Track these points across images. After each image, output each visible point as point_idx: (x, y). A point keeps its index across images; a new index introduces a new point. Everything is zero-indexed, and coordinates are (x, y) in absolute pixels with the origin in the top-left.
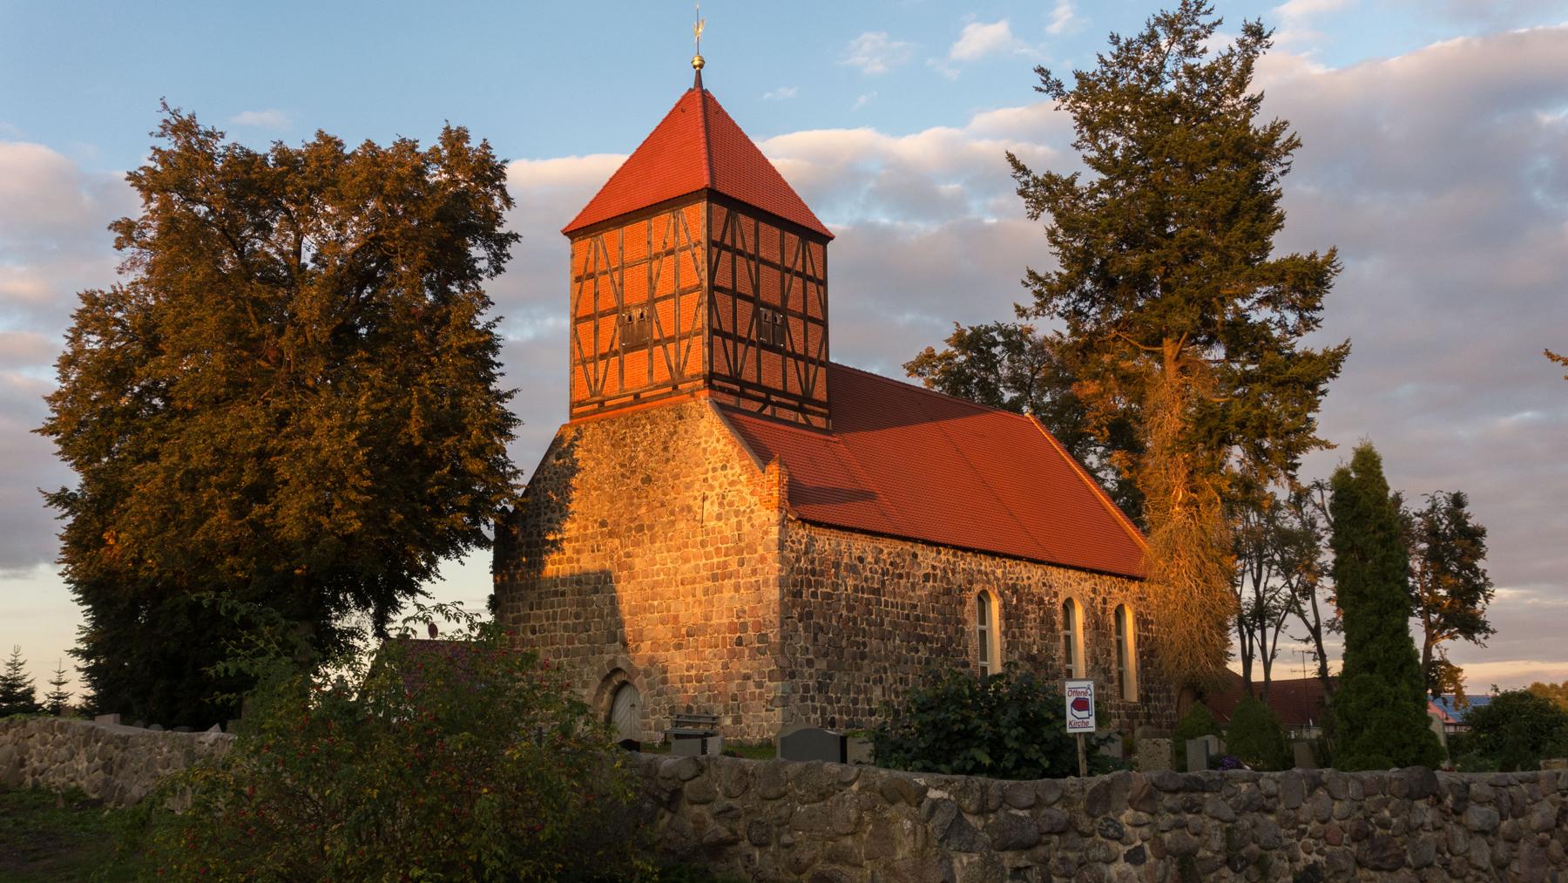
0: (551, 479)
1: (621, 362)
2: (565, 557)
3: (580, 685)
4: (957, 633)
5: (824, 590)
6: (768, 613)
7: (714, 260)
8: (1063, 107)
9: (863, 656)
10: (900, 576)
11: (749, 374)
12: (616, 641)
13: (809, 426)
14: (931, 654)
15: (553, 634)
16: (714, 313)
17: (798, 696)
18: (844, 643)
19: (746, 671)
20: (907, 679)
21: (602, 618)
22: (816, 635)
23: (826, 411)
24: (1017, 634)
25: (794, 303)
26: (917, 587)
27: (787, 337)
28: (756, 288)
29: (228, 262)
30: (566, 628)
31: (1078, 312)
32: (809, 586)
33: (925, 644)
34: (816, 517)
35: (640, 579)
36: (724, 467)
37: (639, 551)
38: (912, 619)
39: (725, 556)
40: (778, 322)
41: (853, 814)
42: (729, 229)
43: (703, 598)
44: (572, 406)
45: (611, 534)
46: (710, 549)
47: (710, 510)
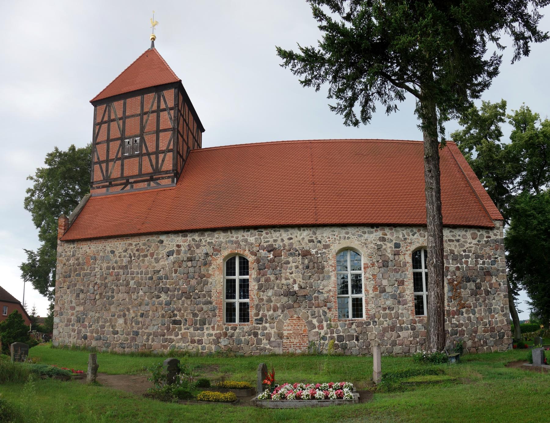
29: (467, 150)
34: (78, 237)
41: (375, 406)
42: (107, 113)
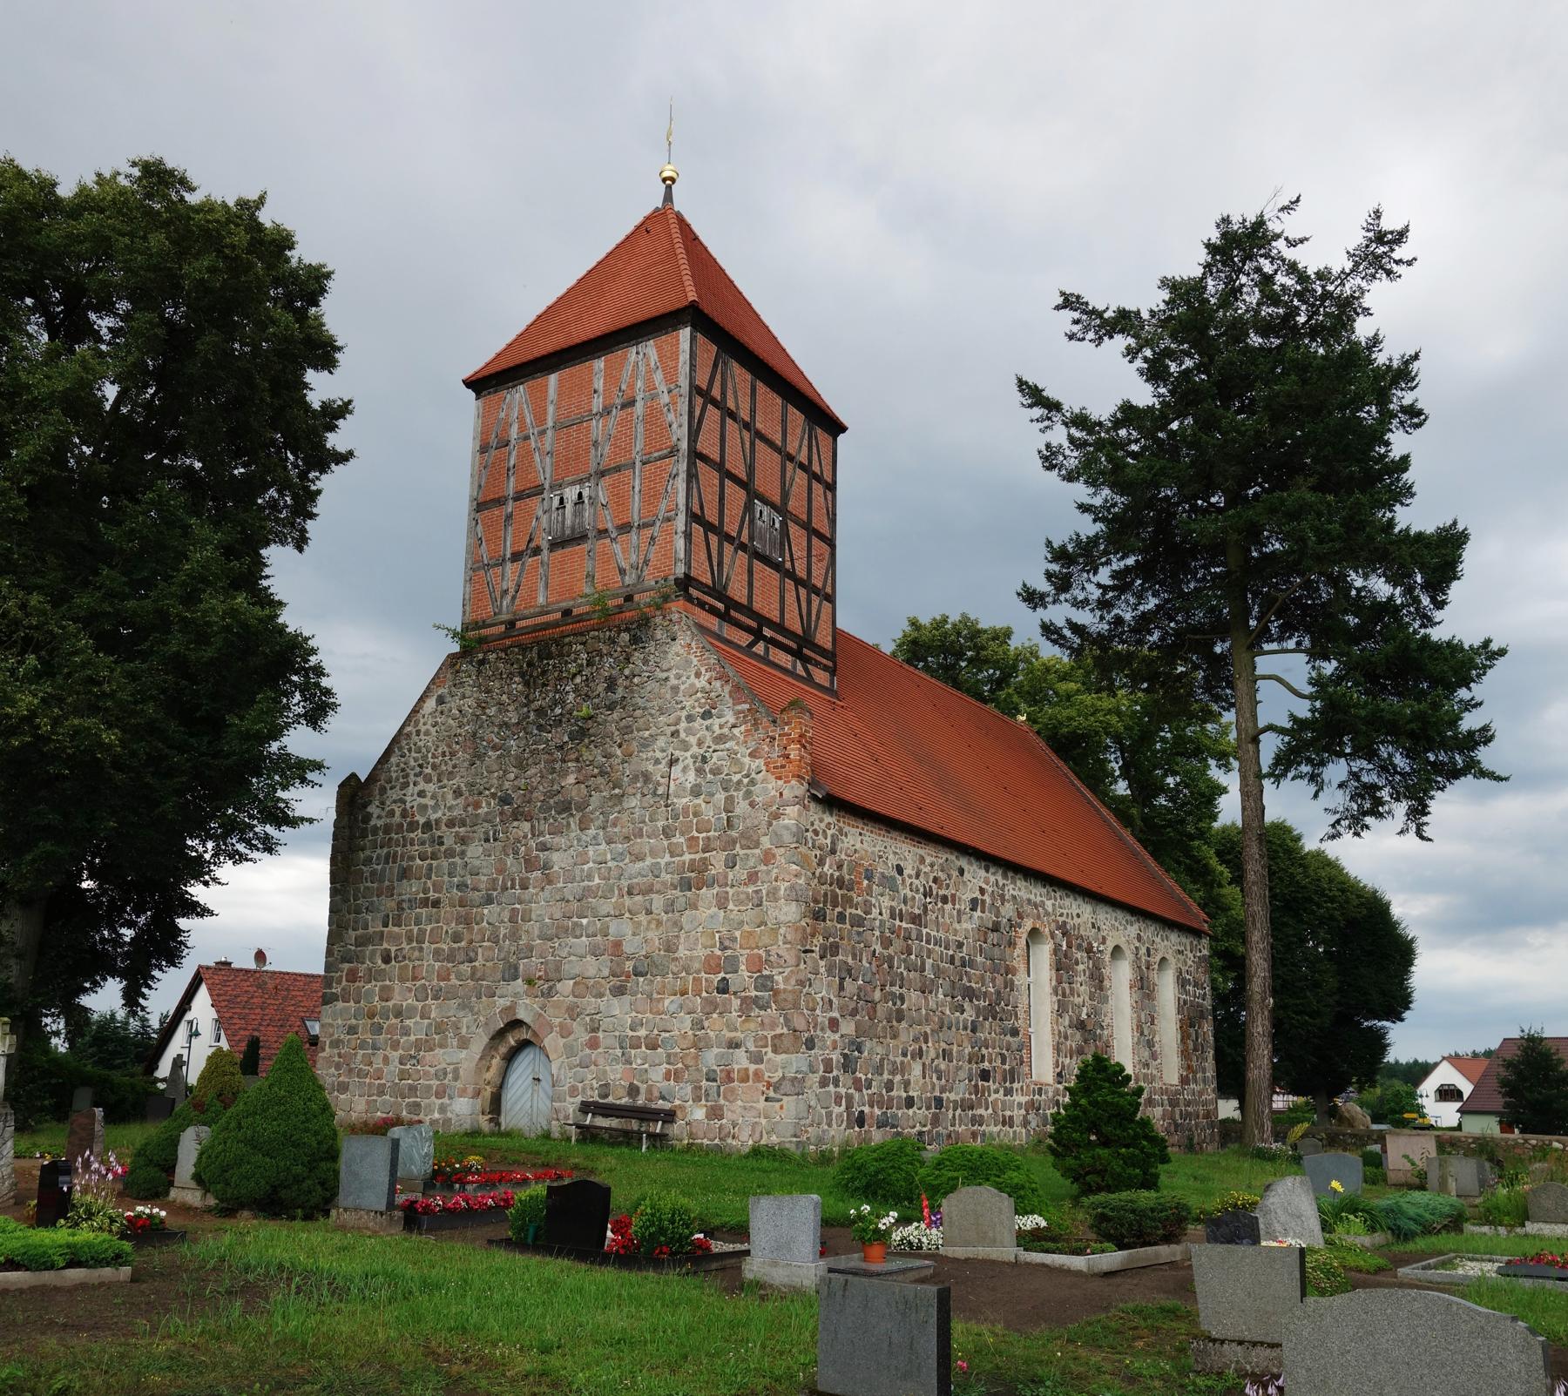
0: (427, 733)
2: (443, 848)
3: (455, 1043)
7: (697, 413)
10: (945, 900)
11: (738, 591)
12: (515, 978)
13: (809, 680)
14: (978, 1017)
16: (695, 490)
17: (816, 1078)
18: (877, 995)
19: (733, 1034)
20: (951, 1053)
21: (497, 943)
22: (842, 979)
24: (1068, 991)
25: (796, 505)
26: (964, 917)
28: (751, 470)
32: (835, 905)
33: (971, 1001)
35: (560, 885)
36: (706, 715)
37: (560, 841)
38: (957, 962)
39: (704, 851)
42: (718, 377)
43: (665, 917)
45: (517, 816)
46: (679, 839)
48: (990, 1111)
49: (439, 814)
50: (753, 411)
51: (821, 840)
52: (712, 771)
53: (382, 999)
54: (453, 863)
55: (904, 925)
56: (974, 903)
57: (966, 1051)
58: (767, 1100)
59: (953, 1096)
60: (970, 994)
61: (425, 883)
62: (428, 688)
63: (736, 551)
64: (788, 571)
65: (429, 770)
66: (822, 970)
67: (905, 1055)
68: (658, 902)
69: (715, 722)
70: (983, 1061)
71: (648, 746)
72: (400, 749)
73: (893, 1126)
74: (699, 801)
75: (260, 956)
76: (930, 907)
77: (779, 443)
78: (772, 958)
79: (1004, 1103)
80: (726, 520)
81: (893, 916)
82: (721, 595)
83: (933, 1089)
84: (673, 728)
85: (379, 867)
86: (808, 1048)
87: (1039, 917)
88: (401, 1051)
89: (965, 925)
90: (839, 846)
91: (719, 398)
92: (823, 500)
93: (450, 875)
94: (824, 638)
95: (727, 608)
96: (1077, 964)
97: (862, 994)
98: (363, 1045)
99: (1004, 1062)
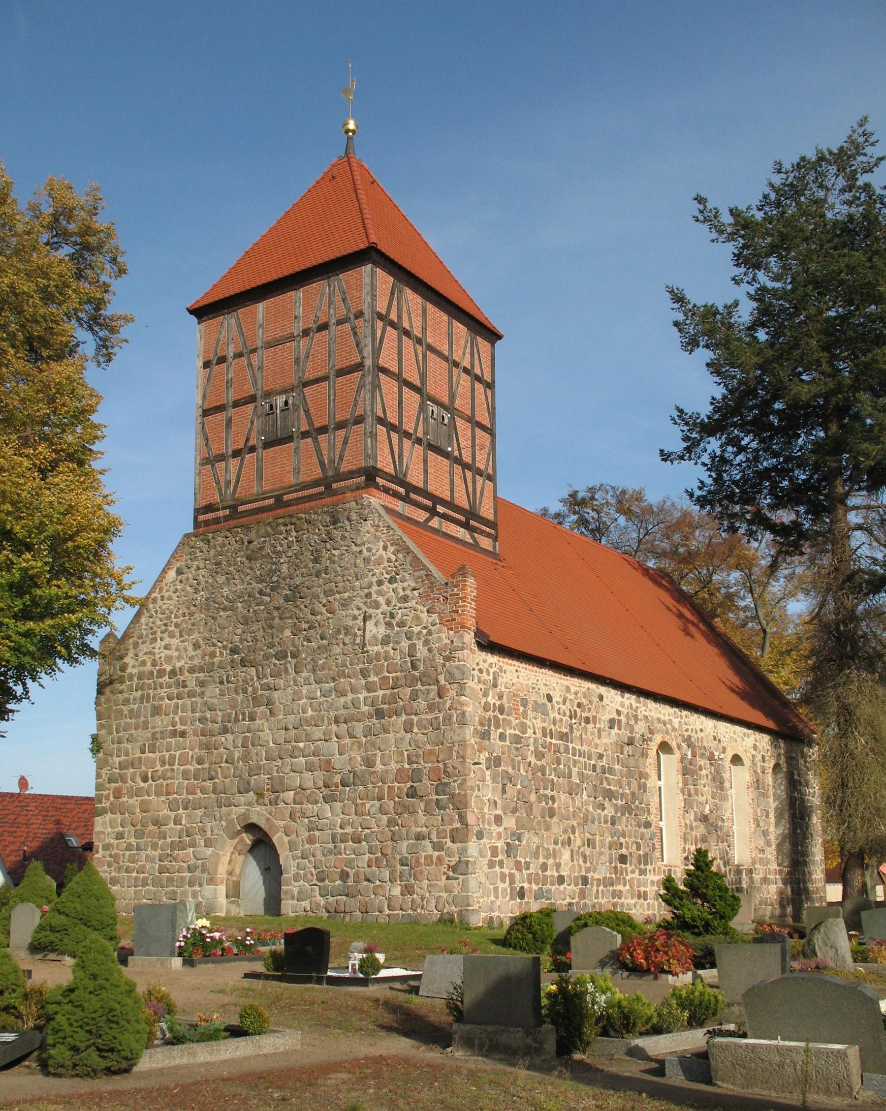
0: (170, 599)
1: (259, 460)
3: (202, 844)
4: (639, 789)
5: (512, 732)
6: (451, 757)
8: (721, 239)
9: (552, 813)
10: (587, 720)
11: (415, 478)
14: (616, 813)
15: (170, 781)
17: (485, 861)
18: (533, 797)
19: (419, 829)
20: (594, 840)
22: (504, 785)
23: (493, 532)
24: (693, 792)
26: (603, 734)
27: (455, 442)
28: (423, 376)
30: (185, 775)
31: (723, 460)
32: (497, 726)
35: (281, 717)
36: (392, 580)
38: (598, 770)
40: (446, 421)
42: (395, 302)
44: (198, 511)
47: (374, 631)
48: (628, 887)
49: (181, 663)
50: (424, 329)
51: (484, 676)
52: (398, 625)
53: (142, 811)
54: (195, 702)
55: (554, 741)
56: (612, 723)
57: (607, 841)
58: (448, 878)
59: (596, 876)
60: (610, 795)
61: (173, 718)
62: (169, 561)
63: (413, 443)
64: (456, 457)
65: (172, 628)
66: (488, 778)
67: (556, 843)
68: (359, 728)
69: (399, 586)
70: (621, 848)
71: (347, 605)
72: (148, 610)
73: (548, 899)
74: (389, 648)
75: (23, 783)
76: (575, 726)
77: (446, 353)
78: (448, 770)
79: (639, 880)
80: (405, 420)
81: (544, 735)
82: (402, 483)
83: (580, 870)
84: (366, 591)
85: (136, 706)
86: (478, 839)
87: (667, 732)
88: (159, 851)
89: (605, 740)
90: (500, 680)
91: (396, 321)
92: (484, 397)
93: (193, 711)
94: (487, 510)
95: (407, 492)
96: (701, 770)
97: (521, 796)
98: (129, 847)
99: (638, 848)
